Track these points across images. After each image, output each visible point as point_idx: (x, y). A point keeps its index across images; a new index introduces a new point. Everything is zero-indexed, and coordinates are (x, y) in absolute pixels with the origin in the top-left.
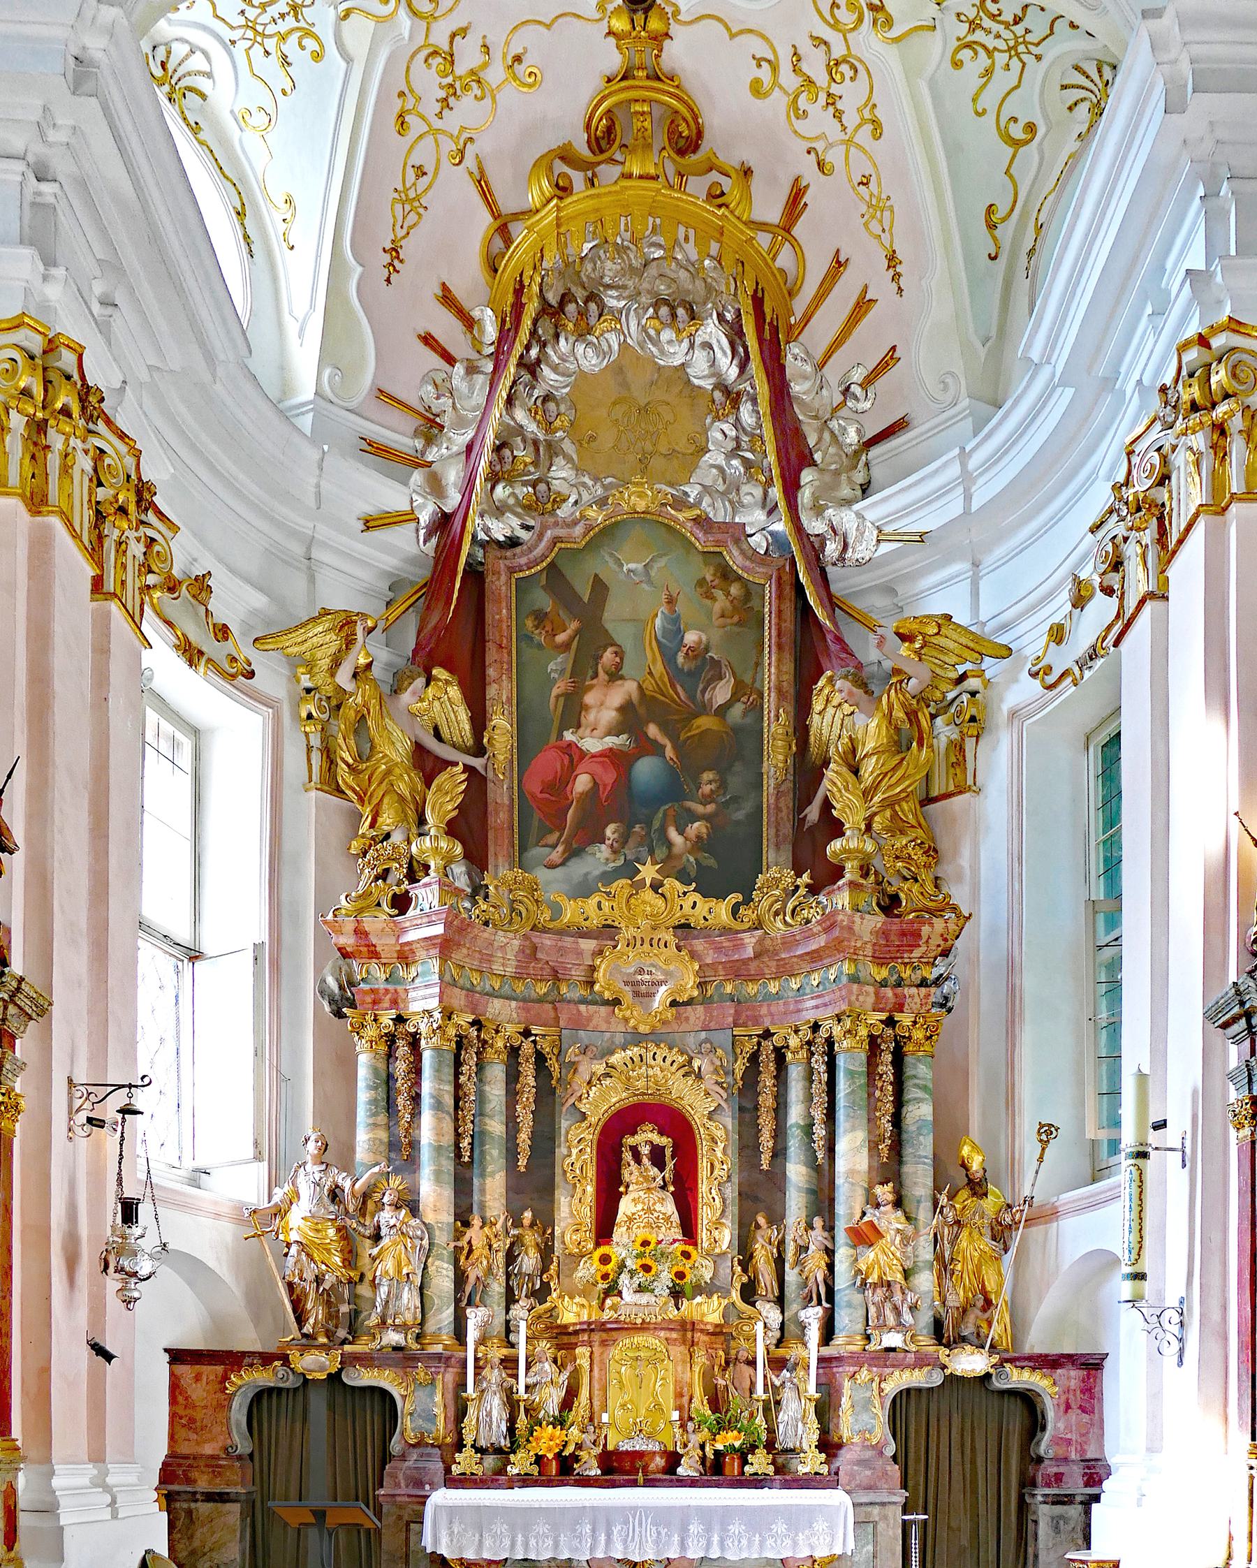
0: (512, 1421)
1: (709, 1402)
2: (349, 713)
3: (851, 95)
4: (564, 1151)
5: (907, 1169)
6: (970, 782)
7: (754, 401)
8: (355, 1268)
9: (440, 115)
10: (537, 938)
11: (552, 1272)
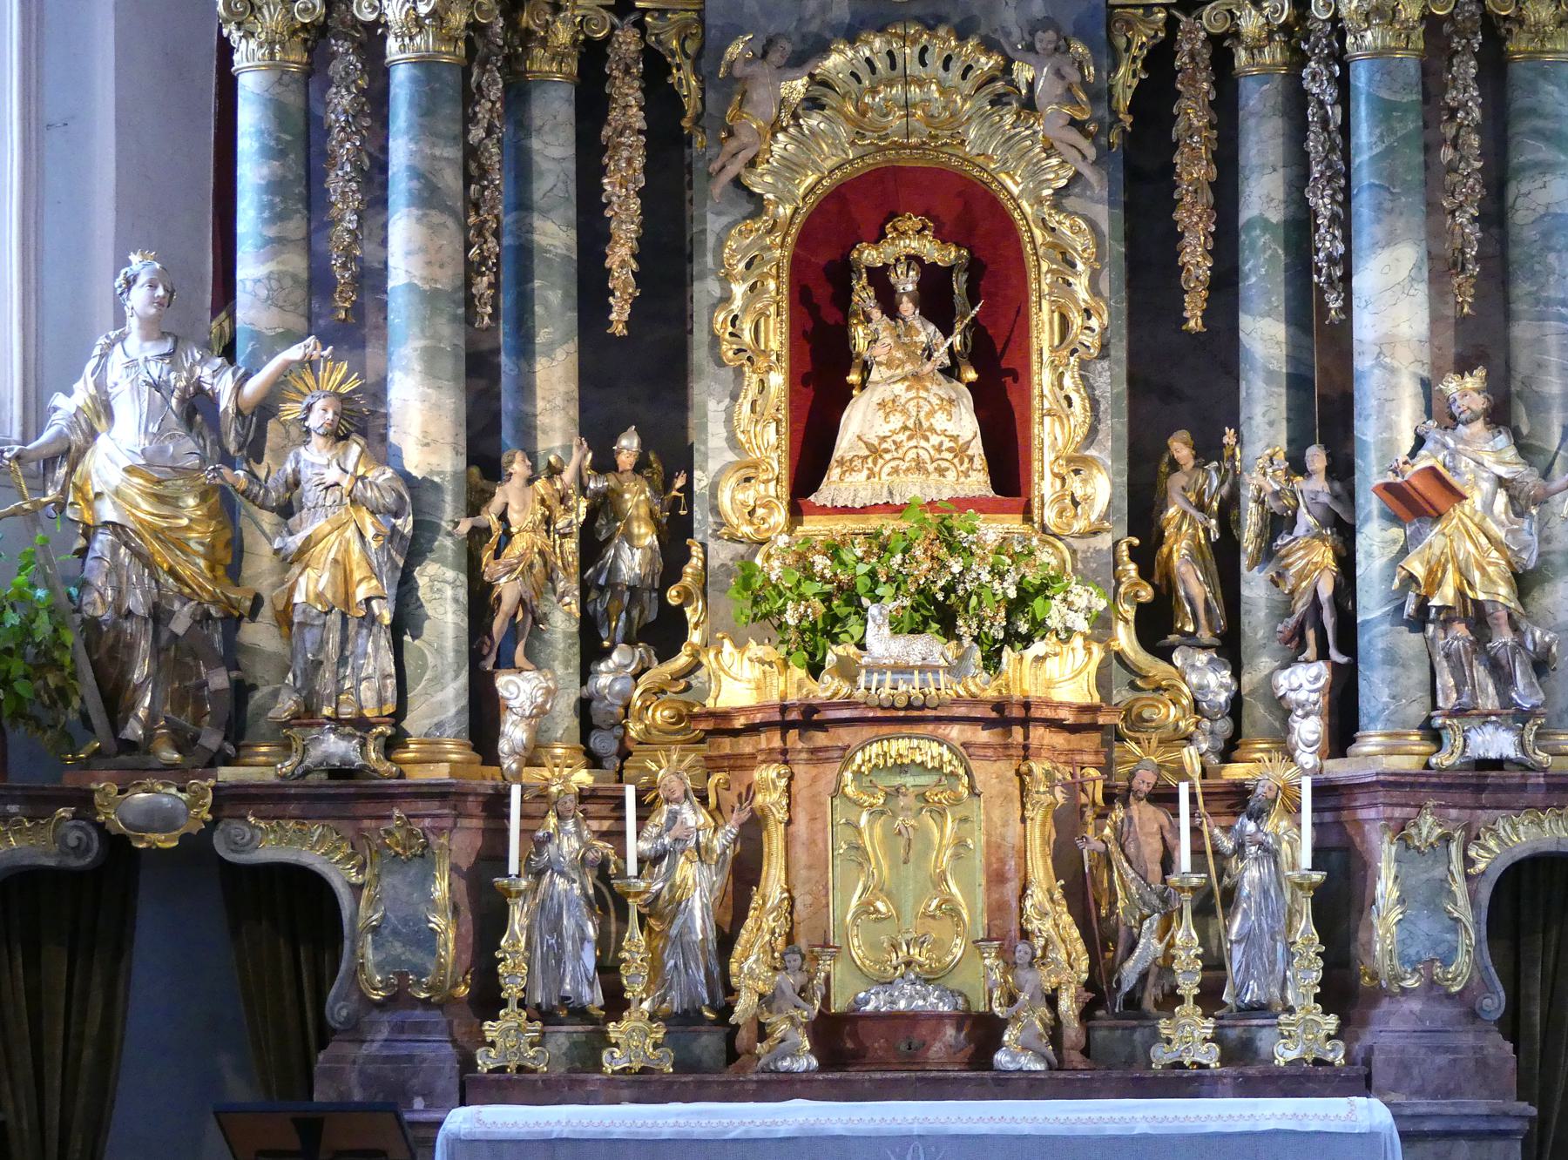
0: (608, 947)
1: (1068, 893)
4: (713, 287)
5: (1521, 331)
11: (687, 580)
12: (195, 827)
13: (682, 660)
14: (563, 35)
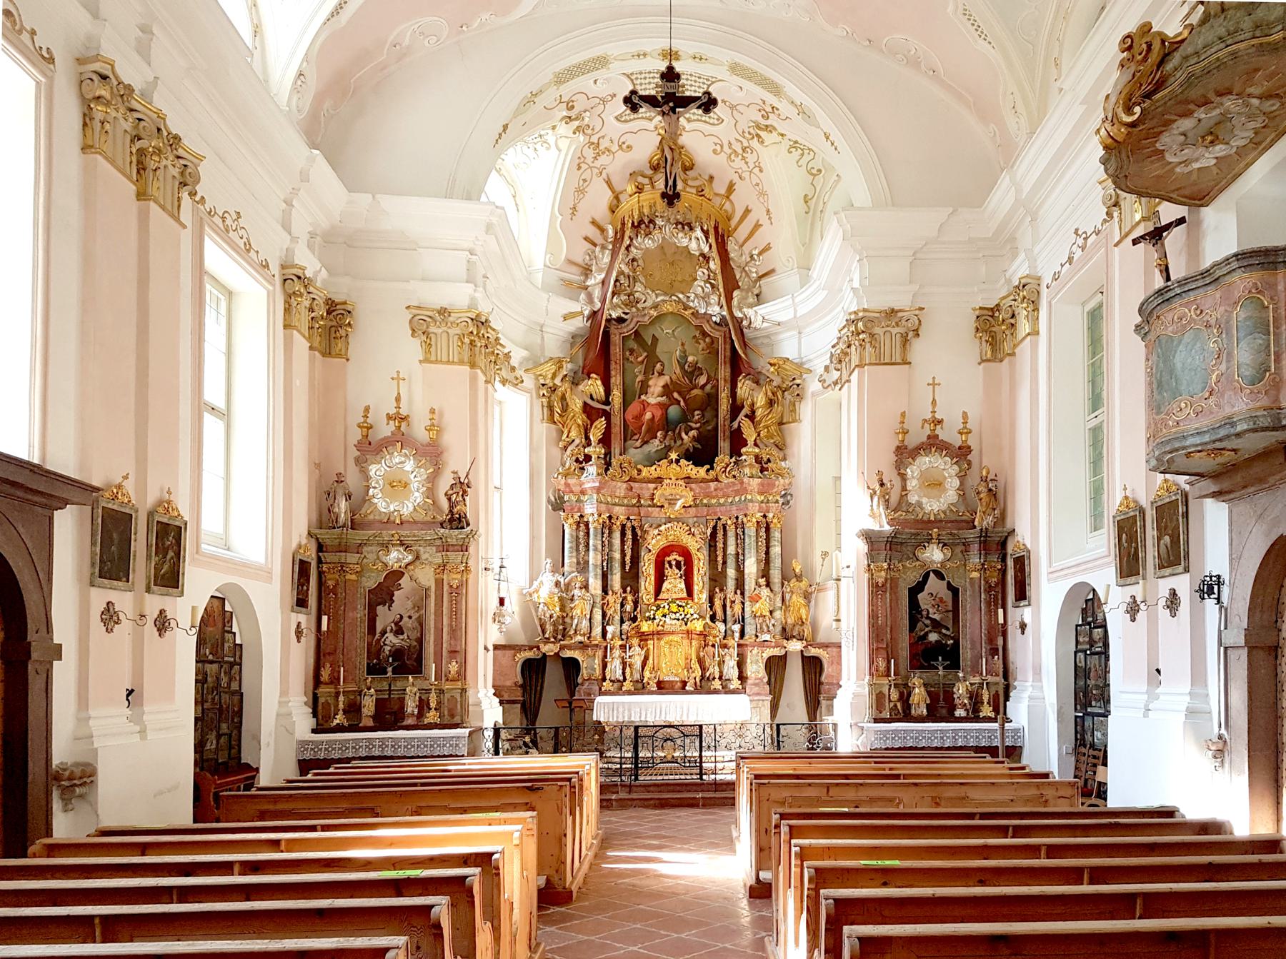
2: (559, 392)
3: (751, 158)
5: (771, 572)
8: (564, 612)
9: (593, 162)
10: (632, 484)
13: (637, 623)
14: (618, 523)
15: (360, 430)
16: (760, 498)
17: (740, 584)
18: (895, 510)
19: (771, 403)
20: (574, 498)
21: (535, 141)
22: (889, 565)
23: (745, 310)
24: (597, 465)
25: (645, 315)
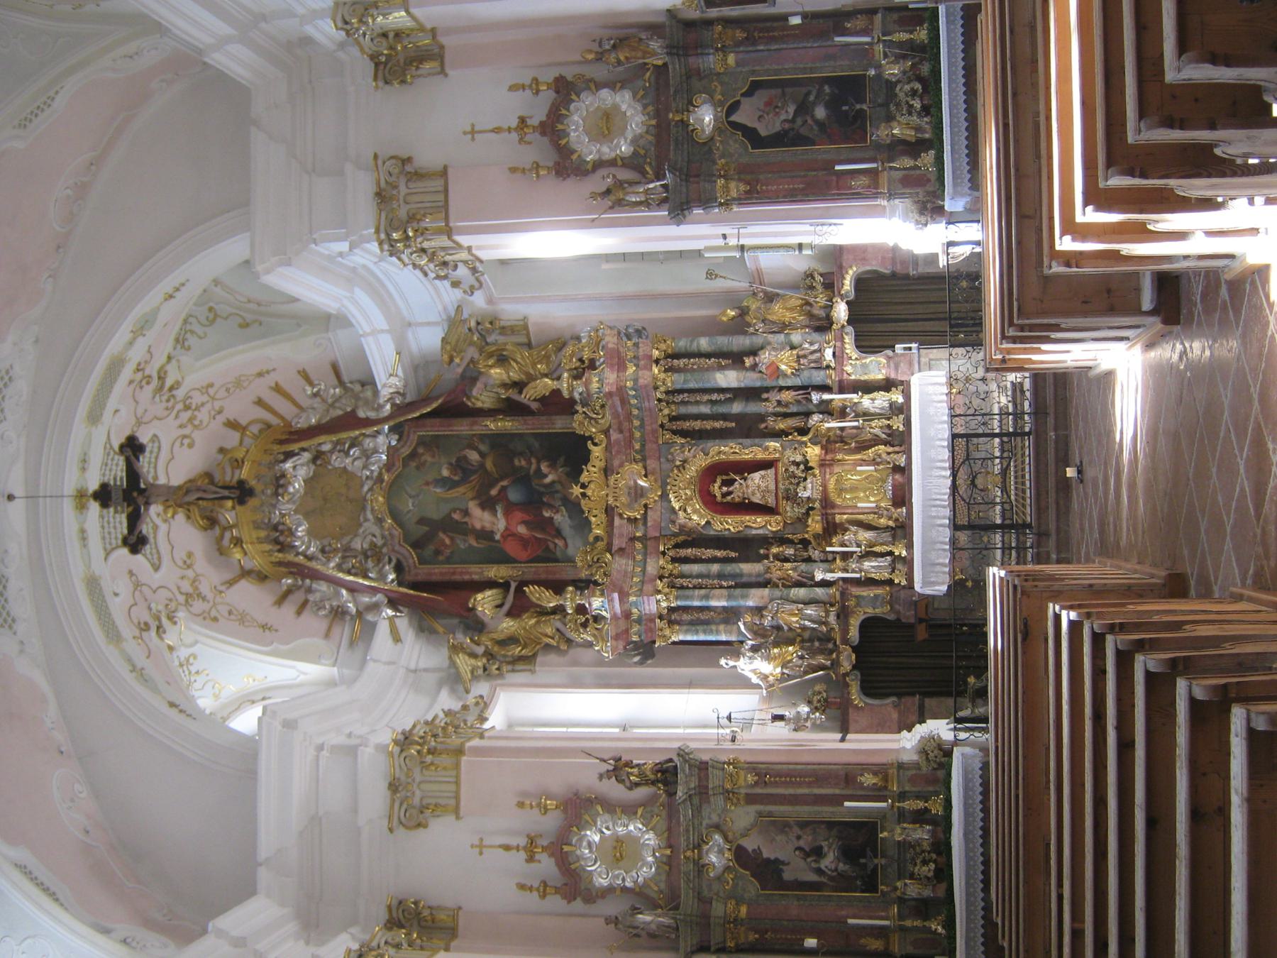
3: (198, 398)
5: (735, 348)
6: (522, 323)
7: (320, 444)
8: (795, 640)
10: (615, 548)
12: (850, 650)
14: (670, 567)
15: (548, 897)
16: (631, 369)
17: (751, 394)
18: (643, 173)
19: (502, 360)
20: (635, 628)
21: (187, 673)
22: (720, 176)
23: (381, 401)
24: (589, 597)
25: (390, 534)
